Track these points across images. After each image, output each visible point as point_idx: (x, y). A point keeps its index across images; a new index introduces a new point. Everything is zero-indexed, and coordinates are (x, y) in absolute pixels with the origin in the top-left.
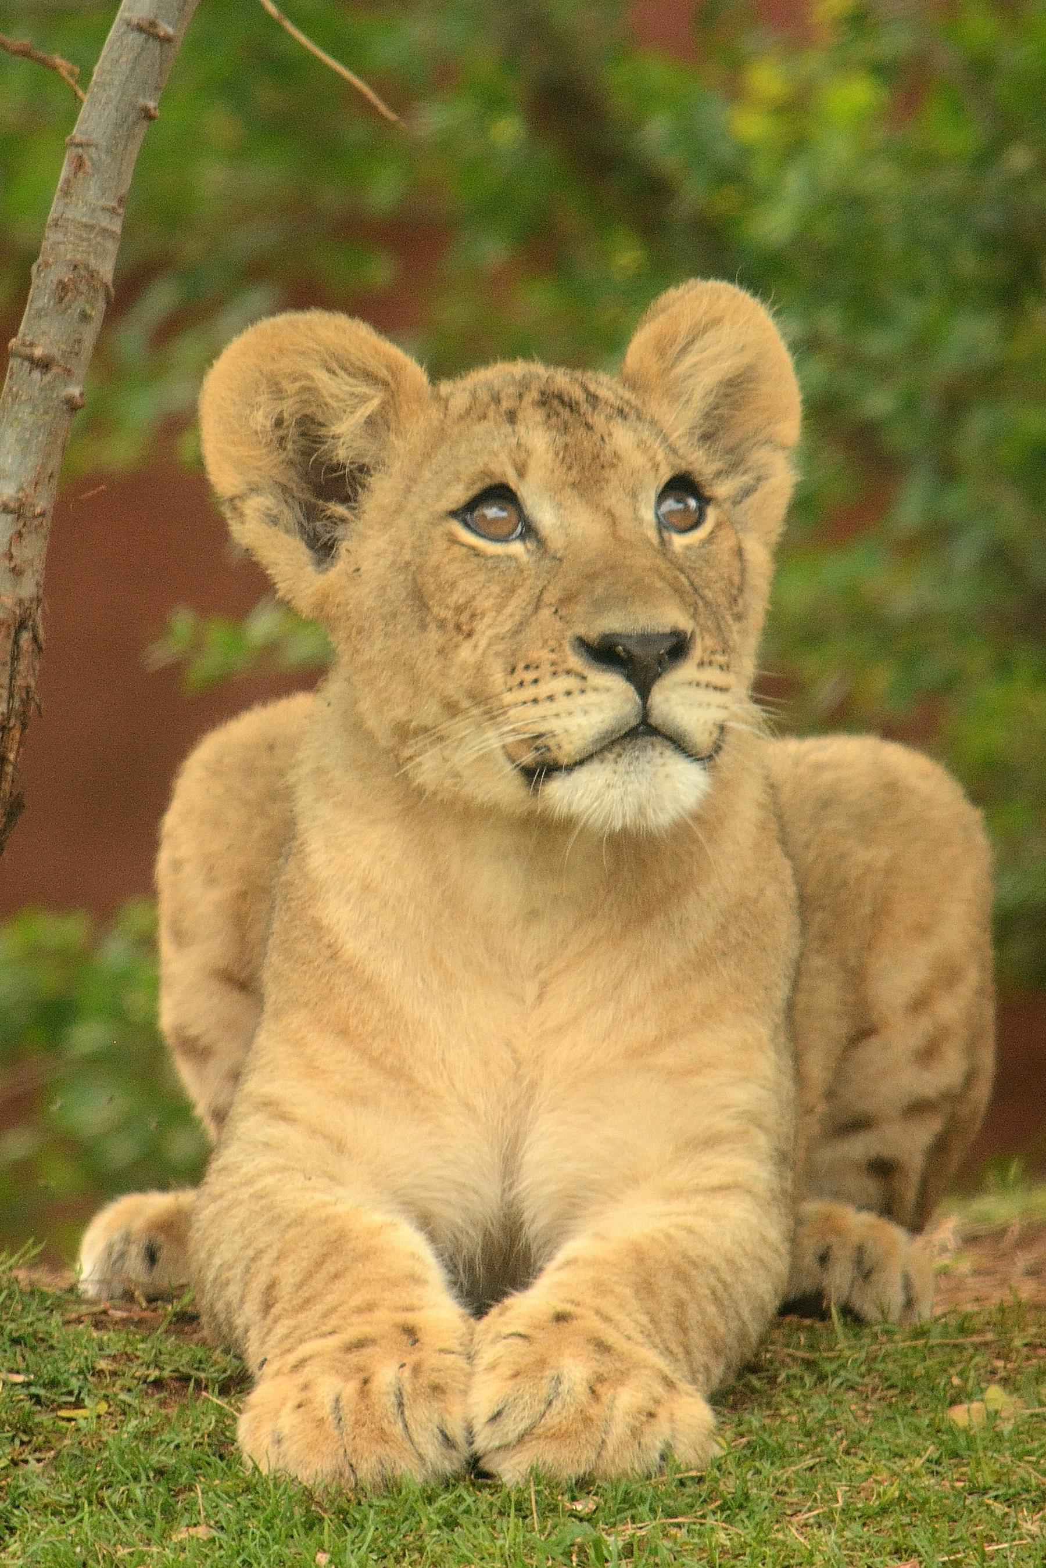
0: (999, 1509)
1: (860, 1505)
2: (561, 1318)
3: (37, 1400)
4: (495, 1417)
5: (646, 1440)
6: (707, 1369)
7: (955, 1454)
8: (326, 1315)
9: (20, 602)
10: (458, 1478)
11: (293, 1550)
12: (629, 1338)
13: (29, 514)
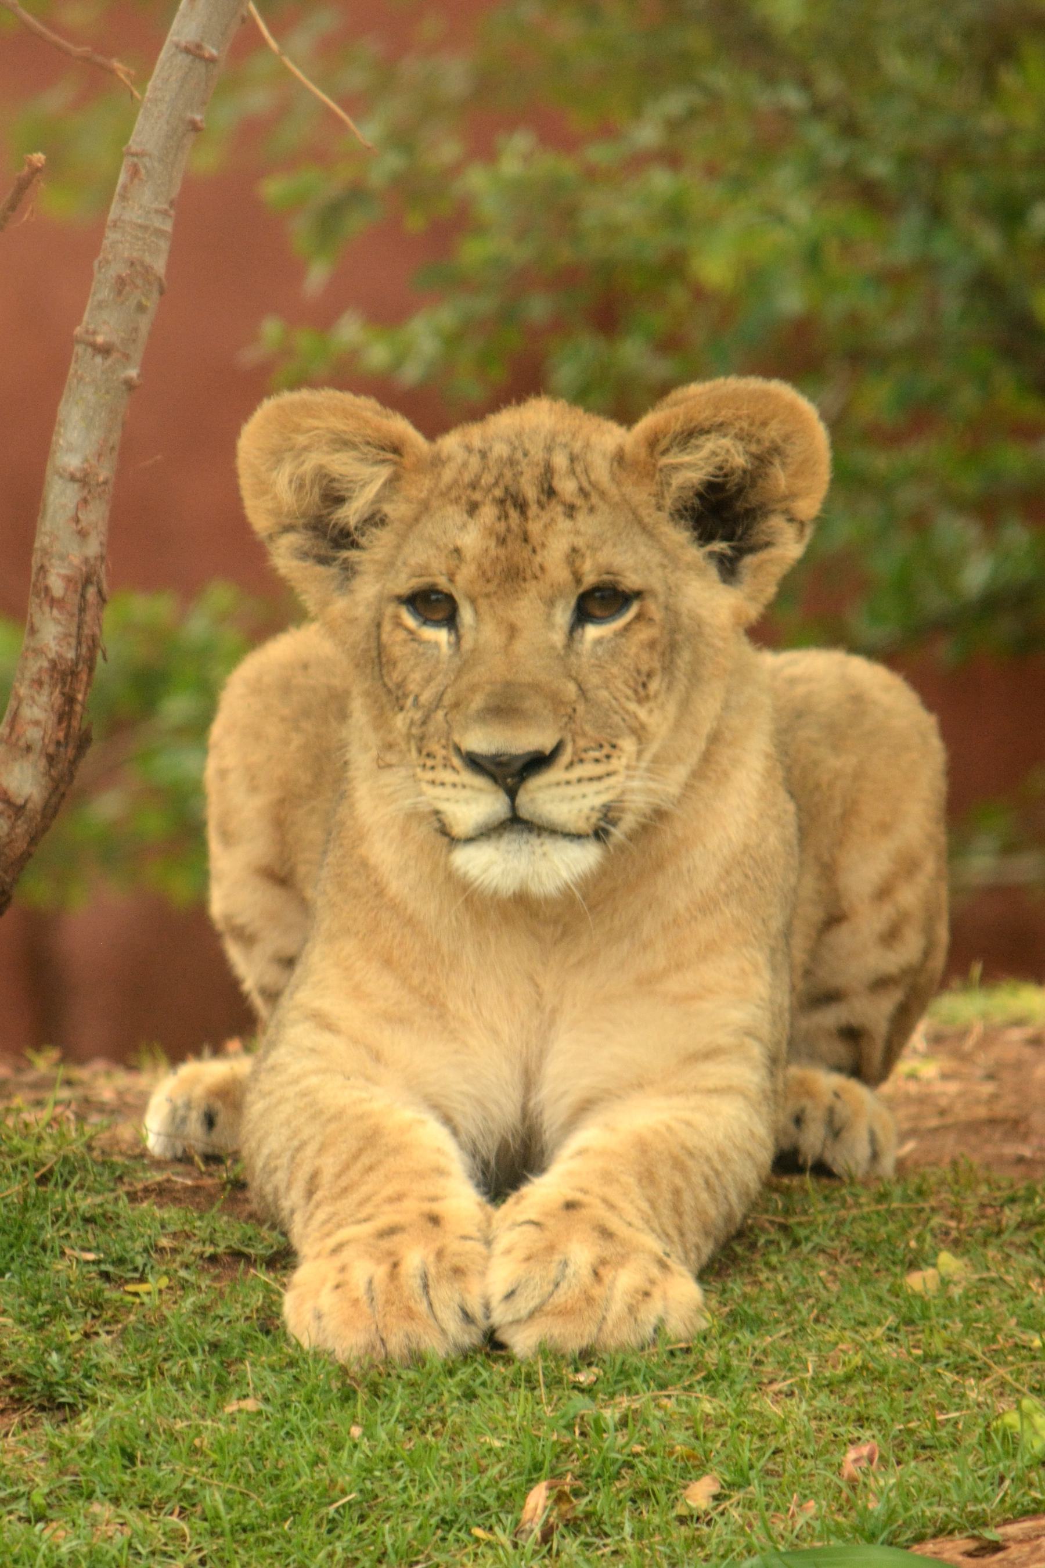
0: (949, 1377)
1: (827, 1374)
2: (570, 1206)
3: (106, 1276)
4: (510, 1295)
5: (641, 1316)
6: (698, 1248)
7: (909, 1322)
8: (361, 1204)
9: (86, 560)
10: (476, 1350)
11: (330, 1422)
12: (630, 1224)
13: (93, 483)
